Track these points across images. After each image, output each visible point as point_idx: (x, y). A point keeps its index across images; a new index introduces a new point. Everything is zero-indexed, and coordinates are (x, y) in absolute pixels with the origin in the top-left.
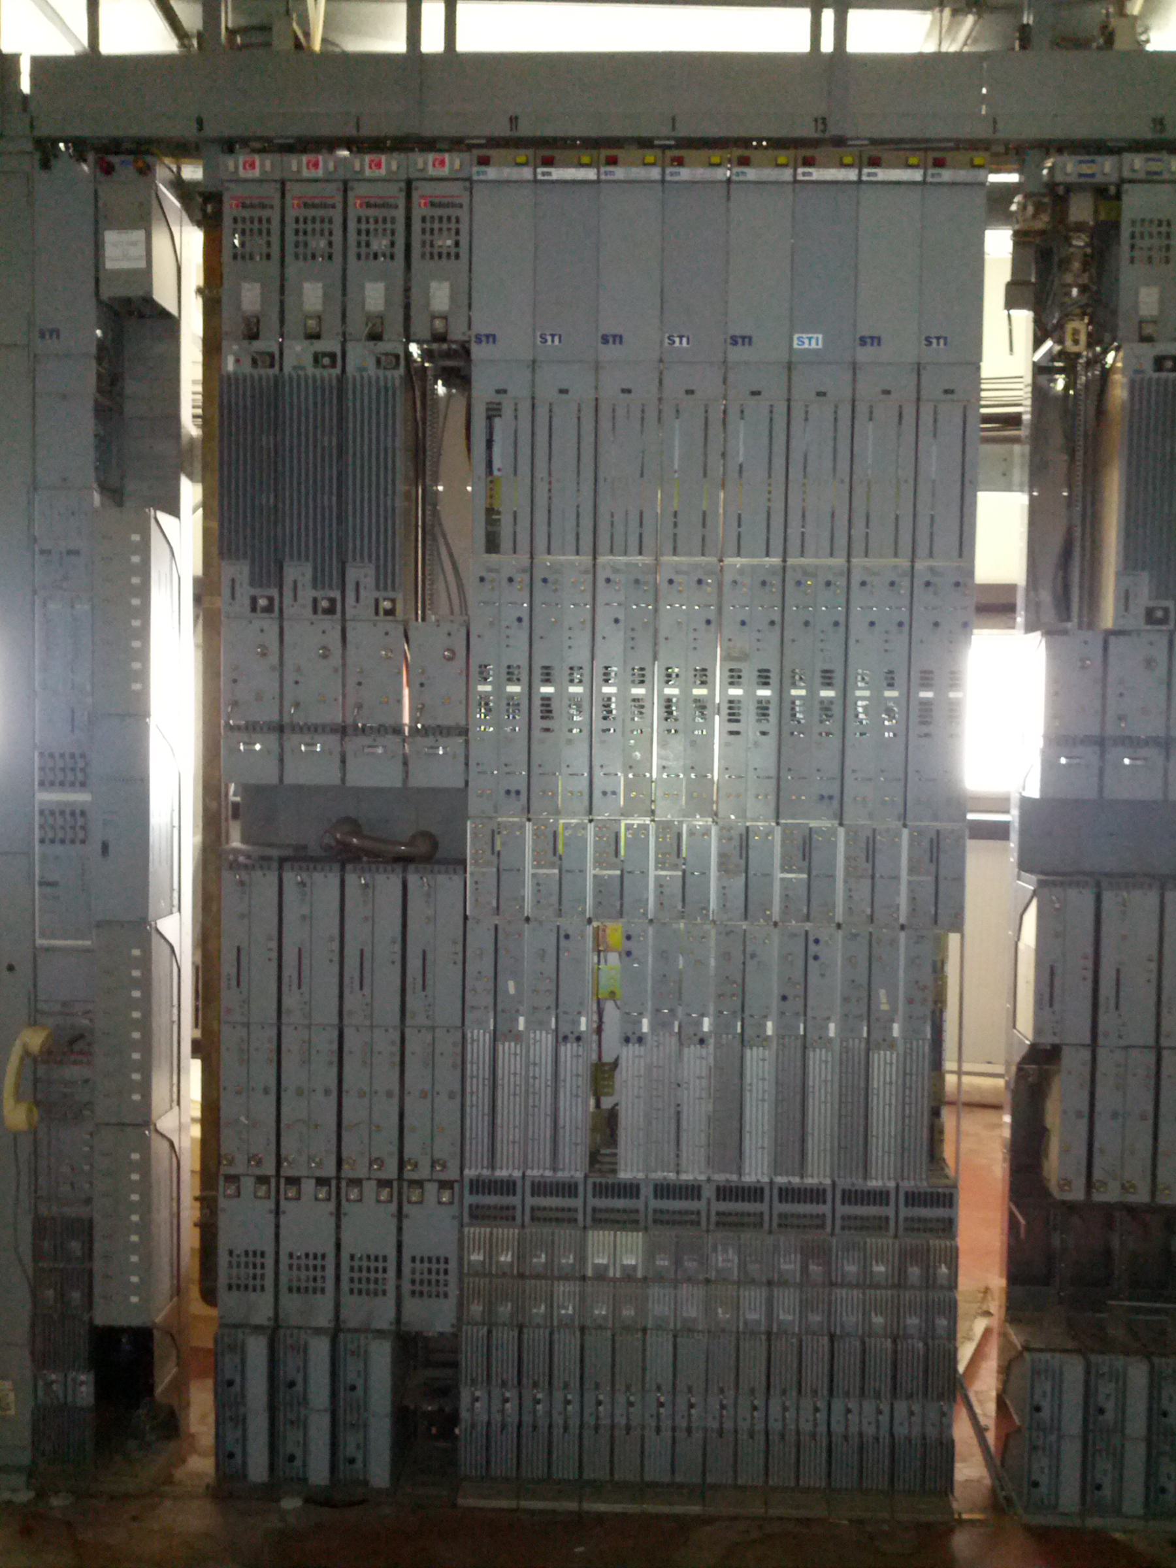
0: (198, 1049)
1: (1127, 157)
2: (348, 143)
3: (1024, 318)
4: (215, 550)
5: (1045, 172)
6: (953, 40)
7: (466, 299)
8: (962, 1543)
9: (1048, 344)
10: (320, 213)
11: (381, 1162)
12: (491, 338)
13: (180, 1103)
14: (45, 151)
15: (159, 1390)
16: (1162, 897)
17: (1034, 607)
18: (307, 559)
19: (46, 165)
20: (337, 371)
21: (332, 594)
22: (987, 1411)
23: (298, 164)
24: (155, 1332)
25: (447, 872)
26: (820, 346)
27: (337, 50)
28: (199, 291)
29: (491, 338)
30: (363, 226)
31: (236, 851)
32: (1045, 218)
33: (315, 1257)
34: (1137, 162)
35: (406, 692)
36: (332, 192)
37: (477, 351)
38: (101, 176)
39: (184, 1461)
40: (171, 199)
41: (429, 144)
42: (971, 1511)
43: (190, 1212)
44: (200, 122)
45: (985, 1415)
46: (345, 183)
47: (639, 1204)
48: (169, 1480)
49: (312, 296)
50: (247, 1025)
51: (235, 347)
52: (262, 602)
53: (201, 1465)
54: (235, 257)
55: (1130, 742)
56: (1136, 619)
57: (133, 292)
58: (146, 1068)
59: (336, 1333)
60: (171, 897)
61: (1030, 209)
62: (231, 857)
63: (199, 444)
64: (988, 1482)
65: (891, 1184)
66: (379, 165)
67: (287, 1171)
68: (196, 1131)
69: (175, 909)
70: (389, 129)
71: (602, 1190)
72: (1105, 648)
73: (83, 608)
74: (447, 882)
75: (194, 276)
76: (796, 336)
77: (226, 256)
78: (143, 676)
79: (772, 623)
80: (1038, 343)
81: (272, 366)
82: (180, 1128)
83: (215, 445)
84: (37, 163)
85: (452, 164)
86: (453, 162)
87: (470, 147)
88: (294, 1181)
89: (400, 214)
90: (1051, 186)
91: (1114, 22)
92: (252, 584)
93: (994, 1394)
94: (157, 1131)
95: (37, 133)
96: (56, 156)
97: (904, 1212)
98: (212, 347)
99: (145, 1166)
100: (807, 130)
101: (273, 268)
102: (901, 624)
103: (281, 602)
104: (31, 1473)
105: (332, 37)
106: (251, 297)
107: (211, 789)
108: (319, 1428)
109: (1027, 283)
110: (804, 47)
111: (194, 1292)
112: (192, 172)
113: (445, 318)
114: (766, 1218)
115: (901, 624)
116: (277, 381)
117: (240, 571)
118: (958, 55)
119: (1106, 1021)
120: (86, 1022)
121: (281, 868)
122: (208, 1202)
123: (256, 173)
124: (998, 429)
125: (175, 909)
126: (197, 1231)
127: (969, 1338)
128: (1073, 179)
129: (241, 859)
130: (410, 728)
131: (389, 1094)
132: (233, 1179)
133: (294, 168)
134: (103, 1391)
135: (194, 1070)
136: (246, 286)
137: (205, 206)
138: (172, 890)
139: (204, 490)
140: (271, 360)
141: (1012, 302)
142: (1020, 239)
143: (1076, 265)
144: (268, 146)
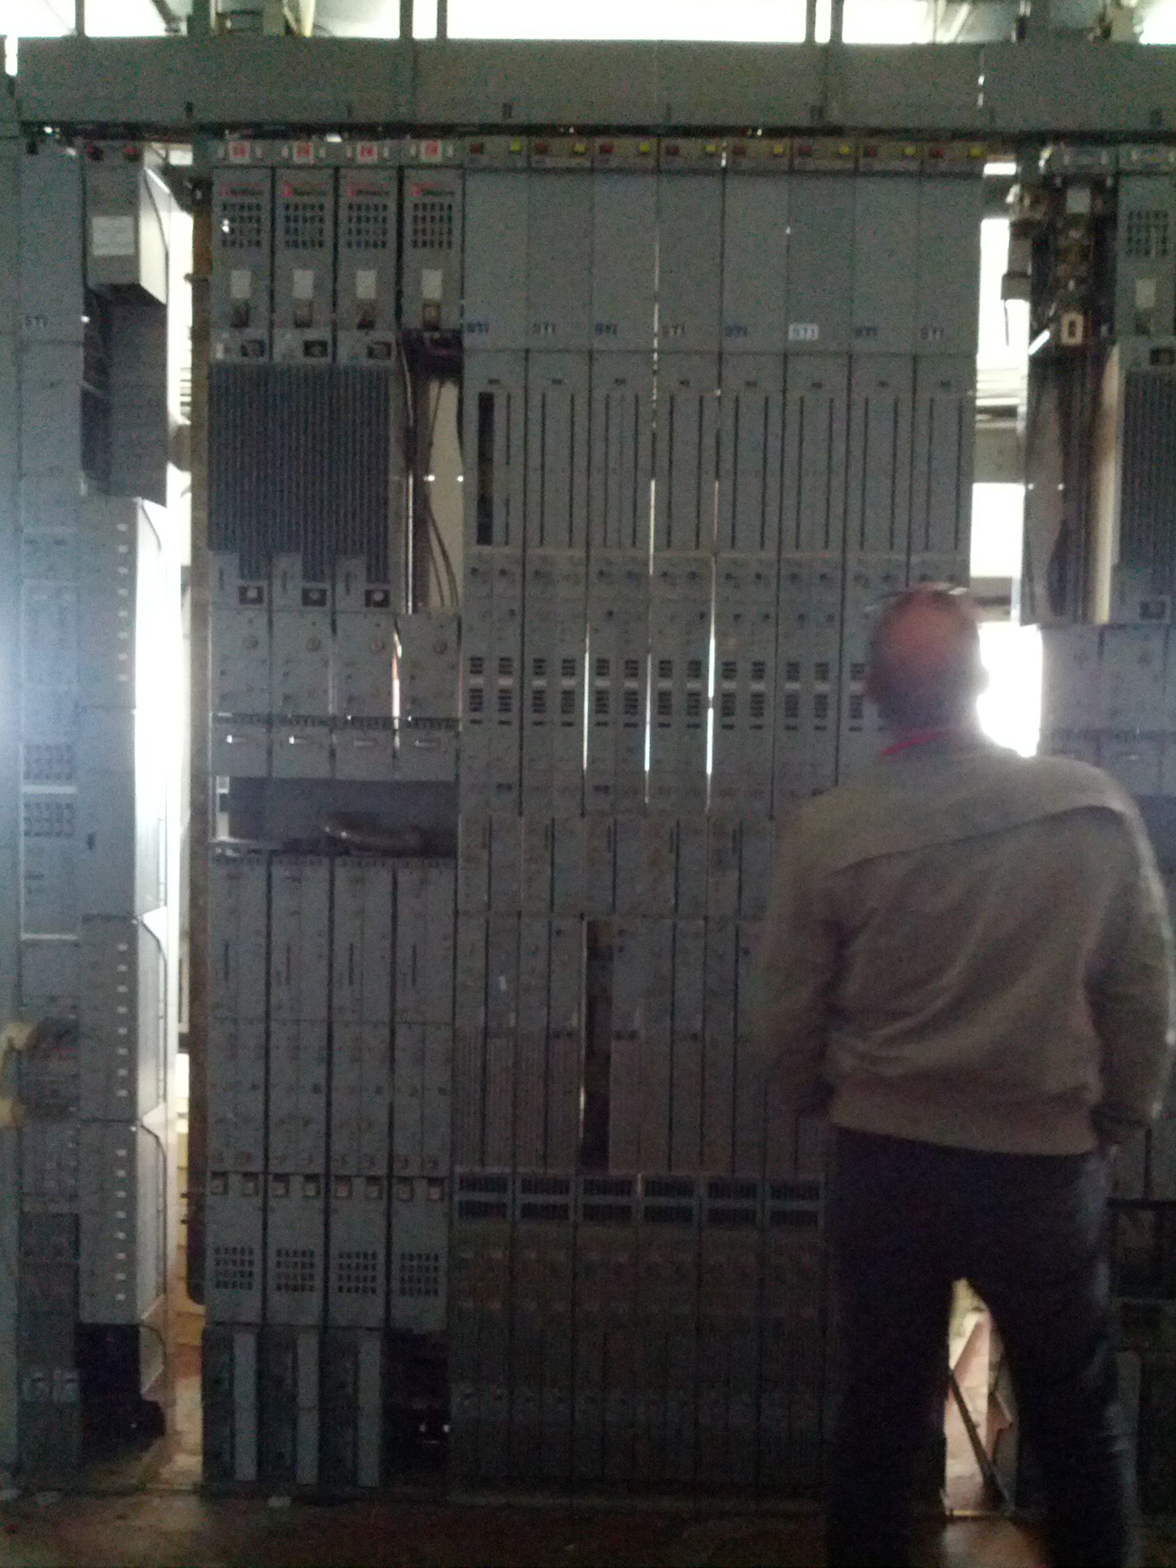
0: (188, 1043)
1: (1123, 149)
2: (338, 129)
3: (1021, 309)
4: (203, 543)
5: (1042, 163)
6: (948, 30)
7: (458, 285)
8: (954, 1539)
9: (1045, 336)
10: (376, 200)
11: (249, 1158)
12: (482, 327)
13: (166, 1101)
14: (32, 133)
15: (144, 1390)
16: (332, 873)
17: (1028, 600)
18: (298, 550)
19: (32, 150)
20: (328, 360)
21: (321, 586)
22: (979, 1406)
23: (293, 151)
24: (142, 1329)
25: (437, 865)
26: (816, 337)
27: (327, 35)
28: (188, 277)
29: (482, 327)
30: (420, 214)
31: (222, 844)
32: (1043, 208)
33: (428, 1258)
34: (1134, 155)
35: (396, 684)
36: (324, 179)
37: (468, 340)
38: (88, 161)
39: (170, 1459)
40: (160, 186)
41: (421, 131)
42: (963, 1507)
43: (177, 1208)
44: (189, 108)
45: (976, 1411)
46: (273, 169)
47: (693, 1202)
48: (155, 1477)
49: (303, 283)
50: (235, 1021)
51: (225, 335)
52: (252, 594)
53: (187, 1462)
54: (224, 243)
55: (300, 721)
56: (1132, 614)
57: (124, 280)
58: (131, 1063)
59: (325, 1328)
60: (158, 892)
61: (1027, 202)
62: (219, 851)
63: (187, 433)
64: (979, 1479)
65: (508, 1170)
66: (370, 152)
67: (275, 1167)
68: (183, 1127)
69: (162, 903)
70: (381, 115)
71: (591, 1187)
72: (1101, 643)
73: (68, 598)
74: (440, 879)
75: (184, 261)
76: (791, 328)
77: (216, 241)
78: (128, 667)
79: (512, 612)
80: (1034, 334)
81: (262, 353)
82: (167, 1124)
83: (204, 434)
84: (24, 148)
85: (253, 151)
86: (441, 150)
87: (462, 135)
88: (282, 1178)
89: (265, 201)
90: (1048, 179)
91: (1111, 13)
92: (306, 576)
93: (985, 1391)
94: (143, 1127)
95: (23, 118)
96: (43, 141)
97: (507, 1198)
98: (200, 335)
99: (131, 1161)
100: (802, 119)
101: (326, 255)
102: (767, 616)
103: (270, 593)
104: (17, 1470)
105: (322, 22)
106: (241, 285)
107: (199, 783)
108: (308, 1425)
109: (1023, 275)
110: (797, 36)
111: (180, 1288)
112: (182, 157)
113: (438, 306)
114: (695, 1212)
115: (767, 616)
116: (332, 371)
117: (230, 561)
118: (951, 47)
119: (280, 995)
120: (72, 1017)
121: (269, 864)
122: (195, 1199)
123: (373, 159)
124: (988, 421)
125: (162, 903)
126: (184, 1228)
127: (960, 1335)
128: (1072, 171)
129: (230, 853)
130: (400, 720)
131: (442, 1091)
132: (222, 1175)
133: (413, 151)
134: (87, 1388)
135: (181, 1065)
136: (235, 274)
137: (192, 191)
138: (158, 884)
139: (193, 480)
140: (262, 347)
141: (1007, 293)
142: (1019, 231)
143: (1072, 257)
144: (258, 131)
